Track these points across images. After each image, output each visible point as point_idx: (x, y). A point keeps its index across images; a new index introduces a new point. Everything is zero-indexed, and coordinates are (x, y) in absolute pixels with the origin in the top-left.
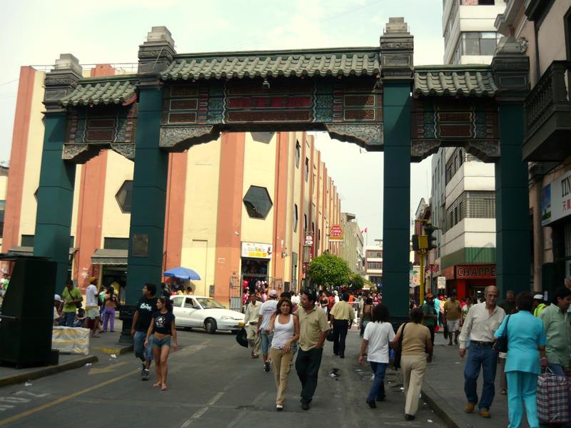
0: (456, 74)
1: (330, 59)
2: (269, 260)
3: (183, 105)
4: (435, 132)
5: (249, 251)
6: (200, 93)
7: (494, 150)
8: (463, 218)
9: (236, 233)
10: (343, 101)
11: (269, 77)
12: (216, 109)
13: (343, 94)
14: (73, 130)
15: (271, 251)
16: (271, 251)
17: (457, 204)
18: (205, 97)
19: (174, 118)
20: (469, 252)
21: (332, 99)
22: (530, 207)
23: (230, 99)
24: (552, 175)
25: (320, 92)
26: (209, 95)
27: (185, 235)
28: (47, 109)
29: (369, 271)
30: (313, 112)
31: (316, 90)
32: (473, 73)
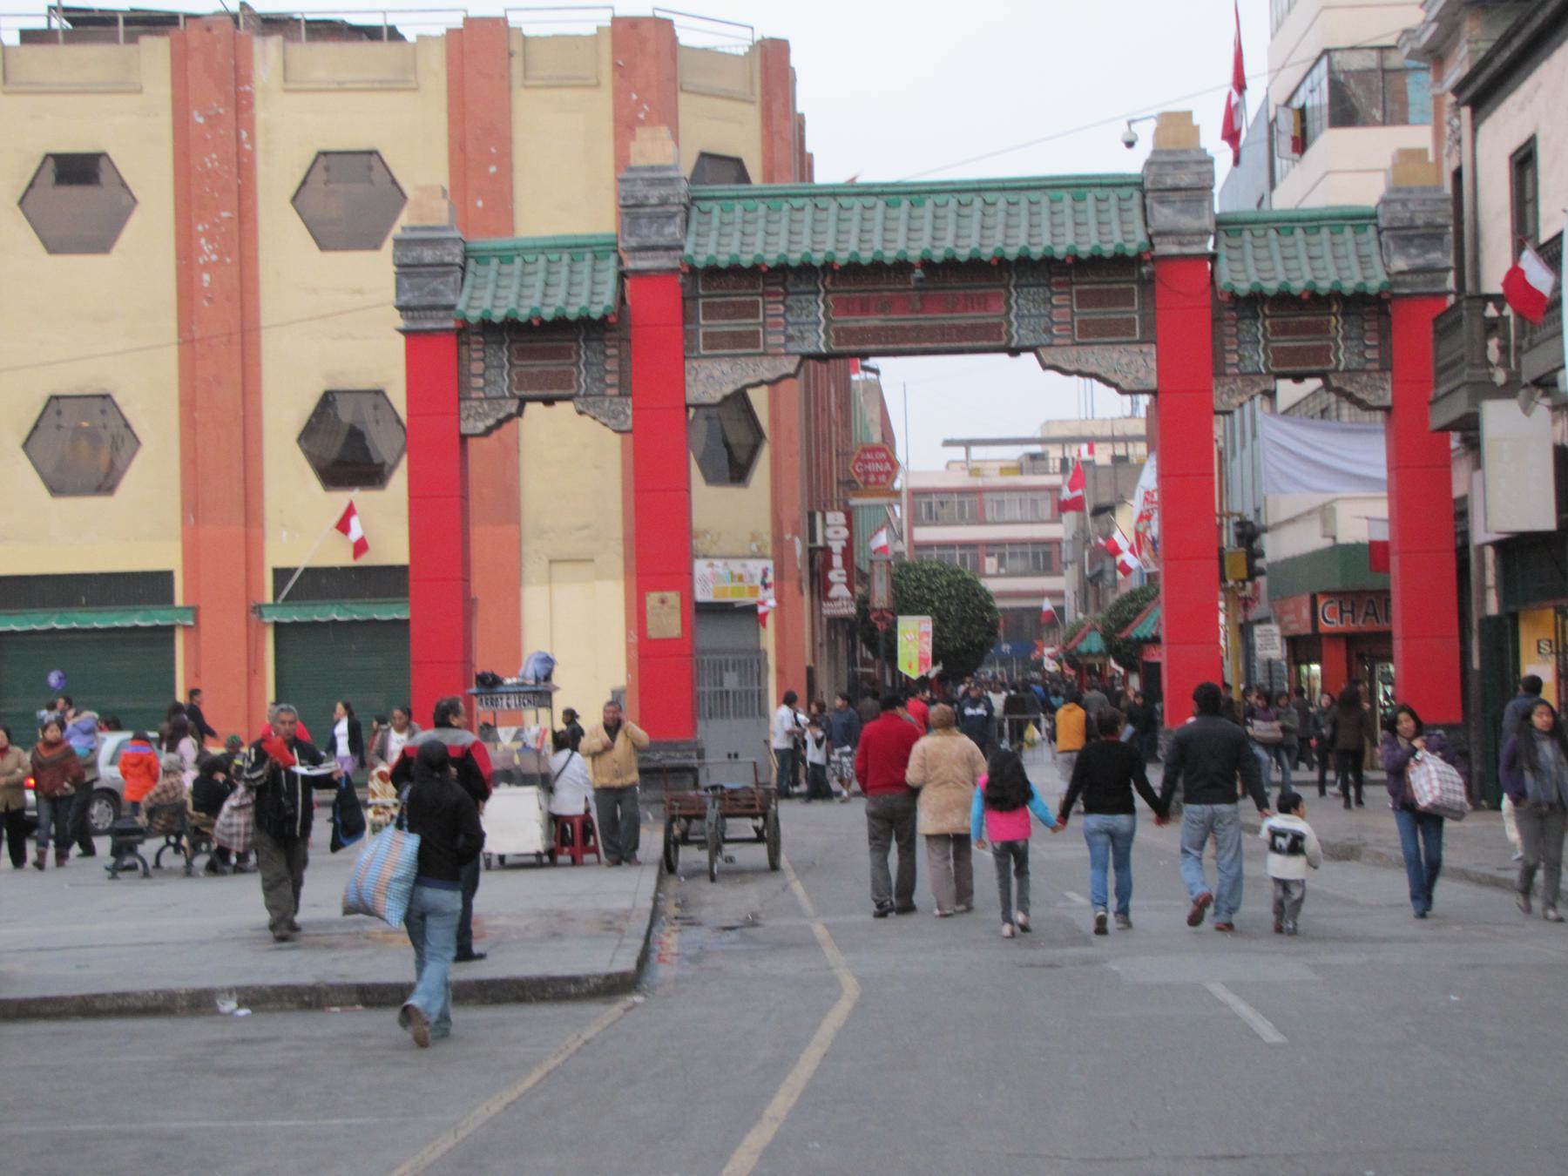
3: (730, 310)
6: (766, 284)
10: (1071, 300)
12: (804, 319)
13: (1072, 283)
15: (770, 578)
18: (777, 294)
19: (713, 340)
21: (1048, 294)
27: (527, 549)
28: (407, 318)
31: (1014, 276)
32: (1336, 230)
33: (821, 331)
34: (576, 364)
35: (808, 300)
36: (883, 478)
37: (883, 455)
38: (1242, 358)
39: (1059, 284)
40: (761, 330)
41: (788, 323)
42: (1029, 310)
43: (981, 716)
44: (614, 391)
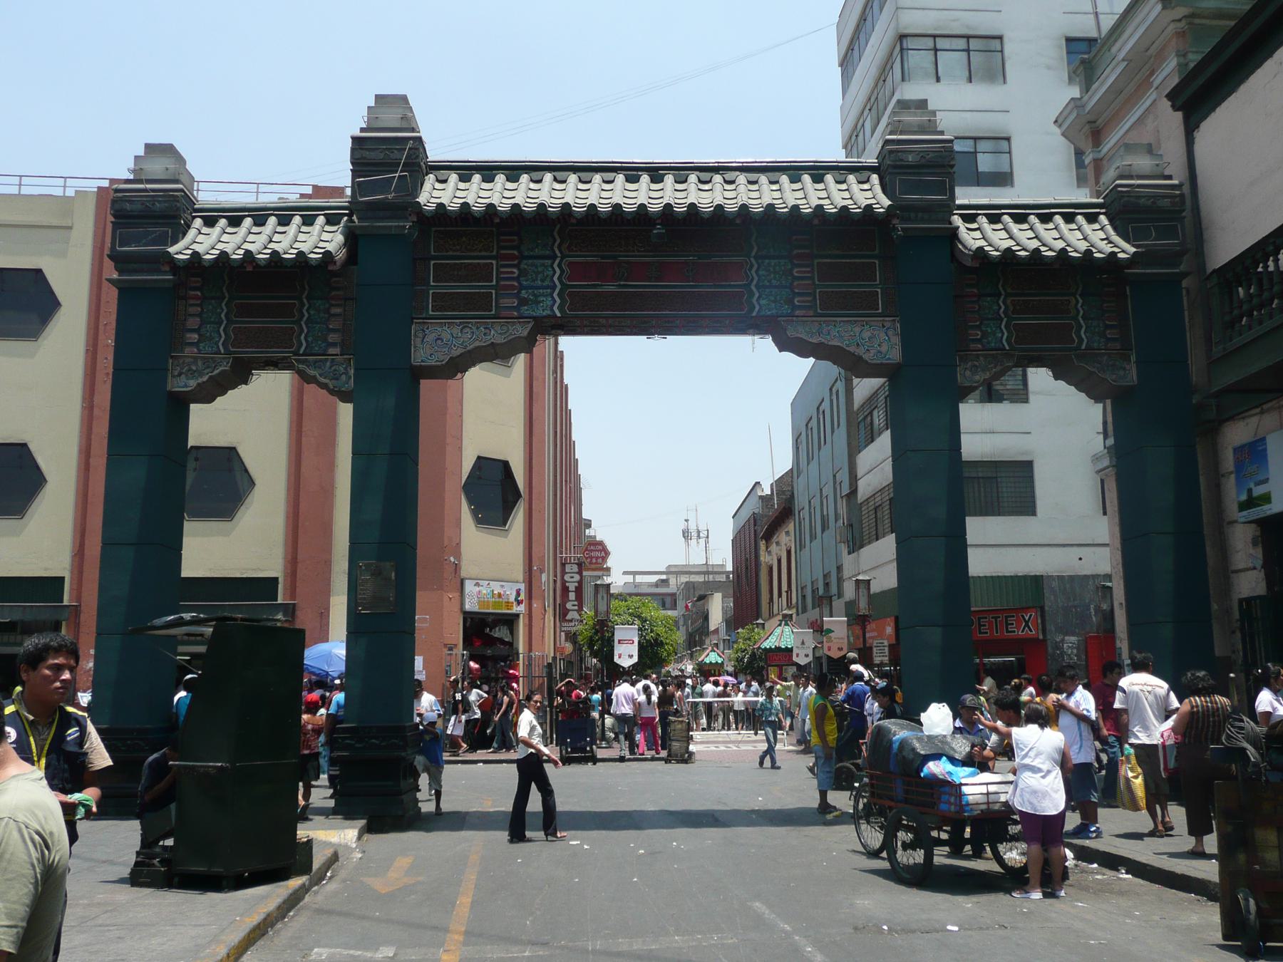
0: (985, 219)
1: (564, 182)
2: (517, 616)
5: (476, 596)
7: (1122, 373)
9: (452, 559)
15: (522, 597)
16: (522, 597)
18: (512, 257)
23: (570, 264)
24: (1255, 420)
30: (751, 294)
33: (555, 295)
34: (298, 322)
35: (543, 265)
36: (600, 560)
37: (600, 547)
38: (985, 335)
40: (494, 292)
41: (521, 287)
42: (769, 281)
43: (1113, 703)
44: (336, 350)
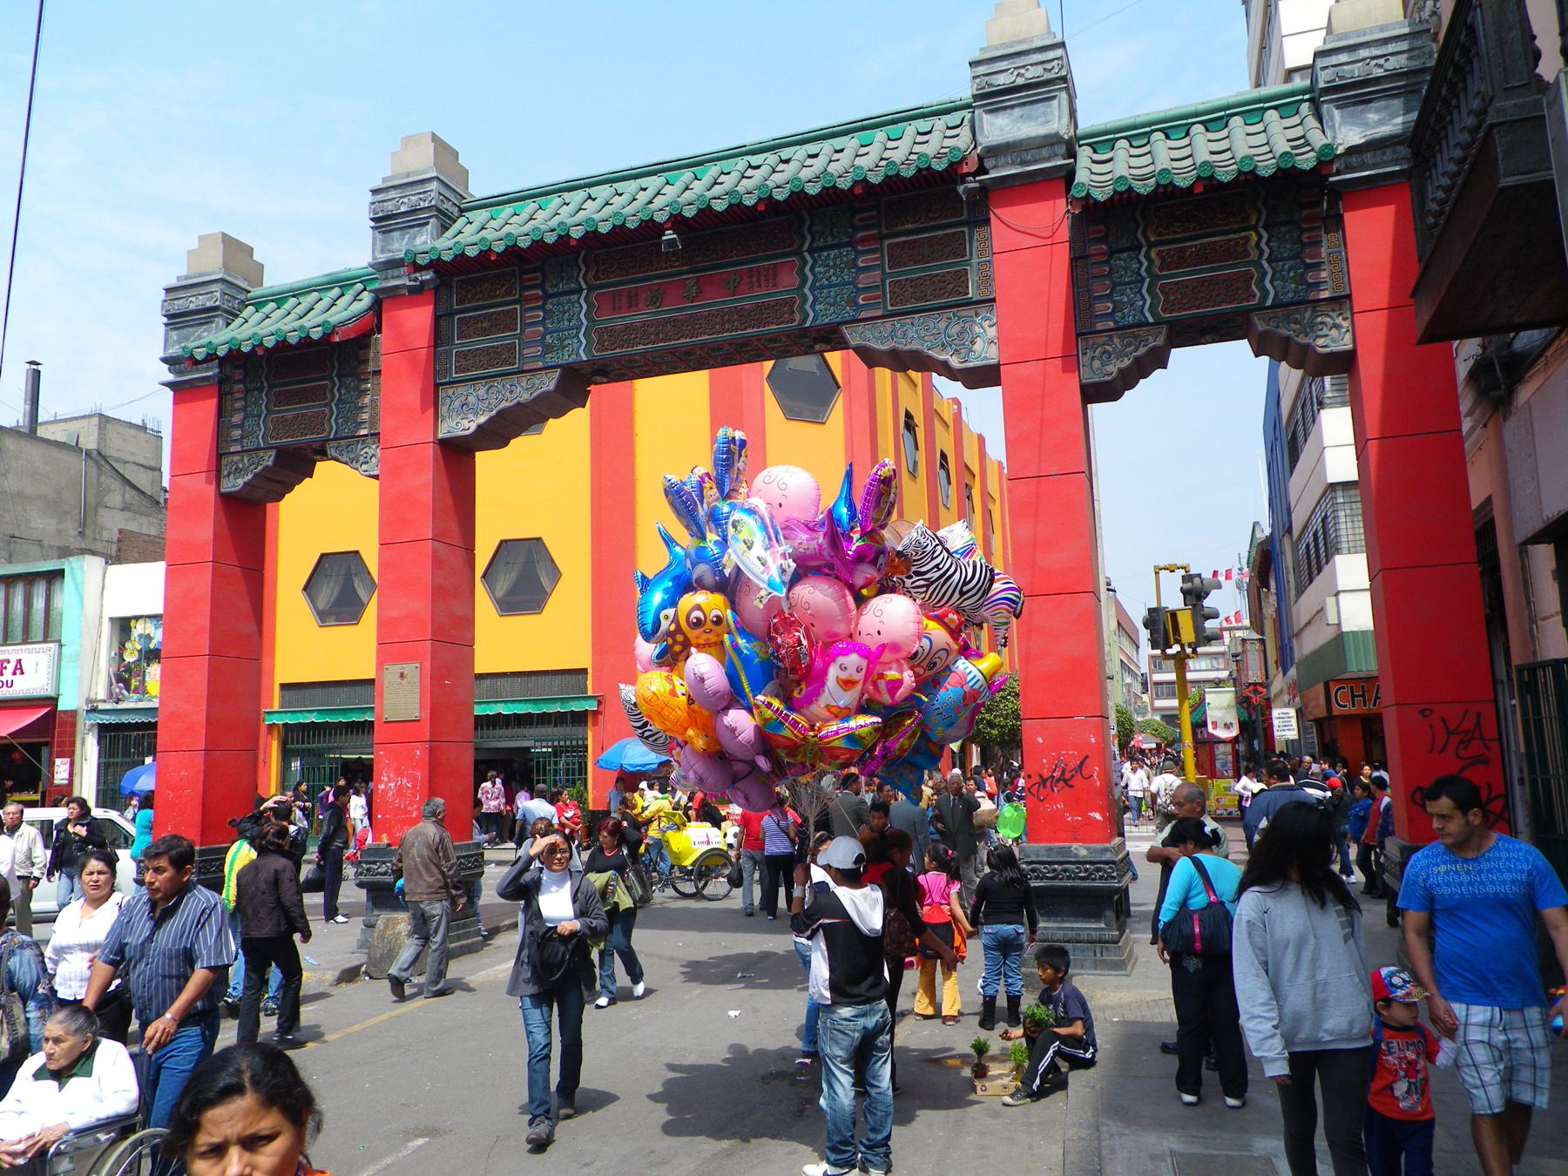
4: (1145, 304)
8: (1333, 555)
11: (677, 221)
14: (237, 418)
17: (1317, 523)
18: (537, 298)
20: (1363, 636)
22: (1476, 501)
25: (821, 243)
26: (544, 291)
29: (1159, 703)
39: (863, 240)
